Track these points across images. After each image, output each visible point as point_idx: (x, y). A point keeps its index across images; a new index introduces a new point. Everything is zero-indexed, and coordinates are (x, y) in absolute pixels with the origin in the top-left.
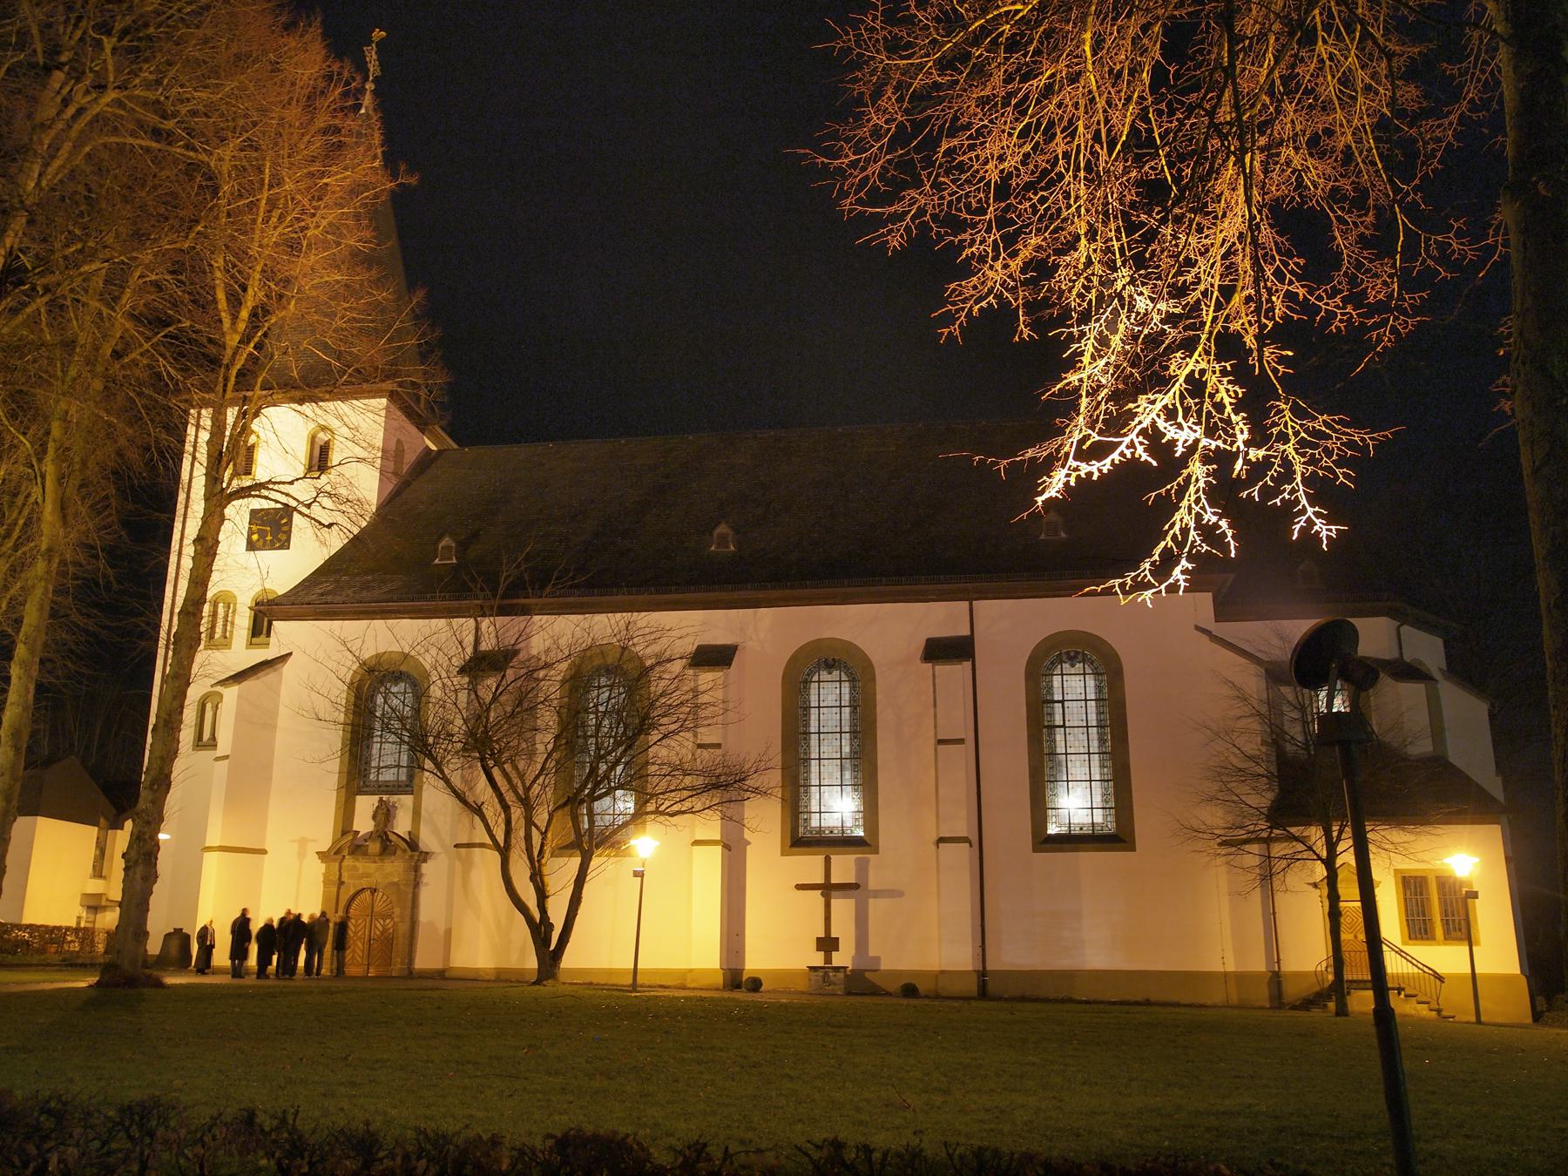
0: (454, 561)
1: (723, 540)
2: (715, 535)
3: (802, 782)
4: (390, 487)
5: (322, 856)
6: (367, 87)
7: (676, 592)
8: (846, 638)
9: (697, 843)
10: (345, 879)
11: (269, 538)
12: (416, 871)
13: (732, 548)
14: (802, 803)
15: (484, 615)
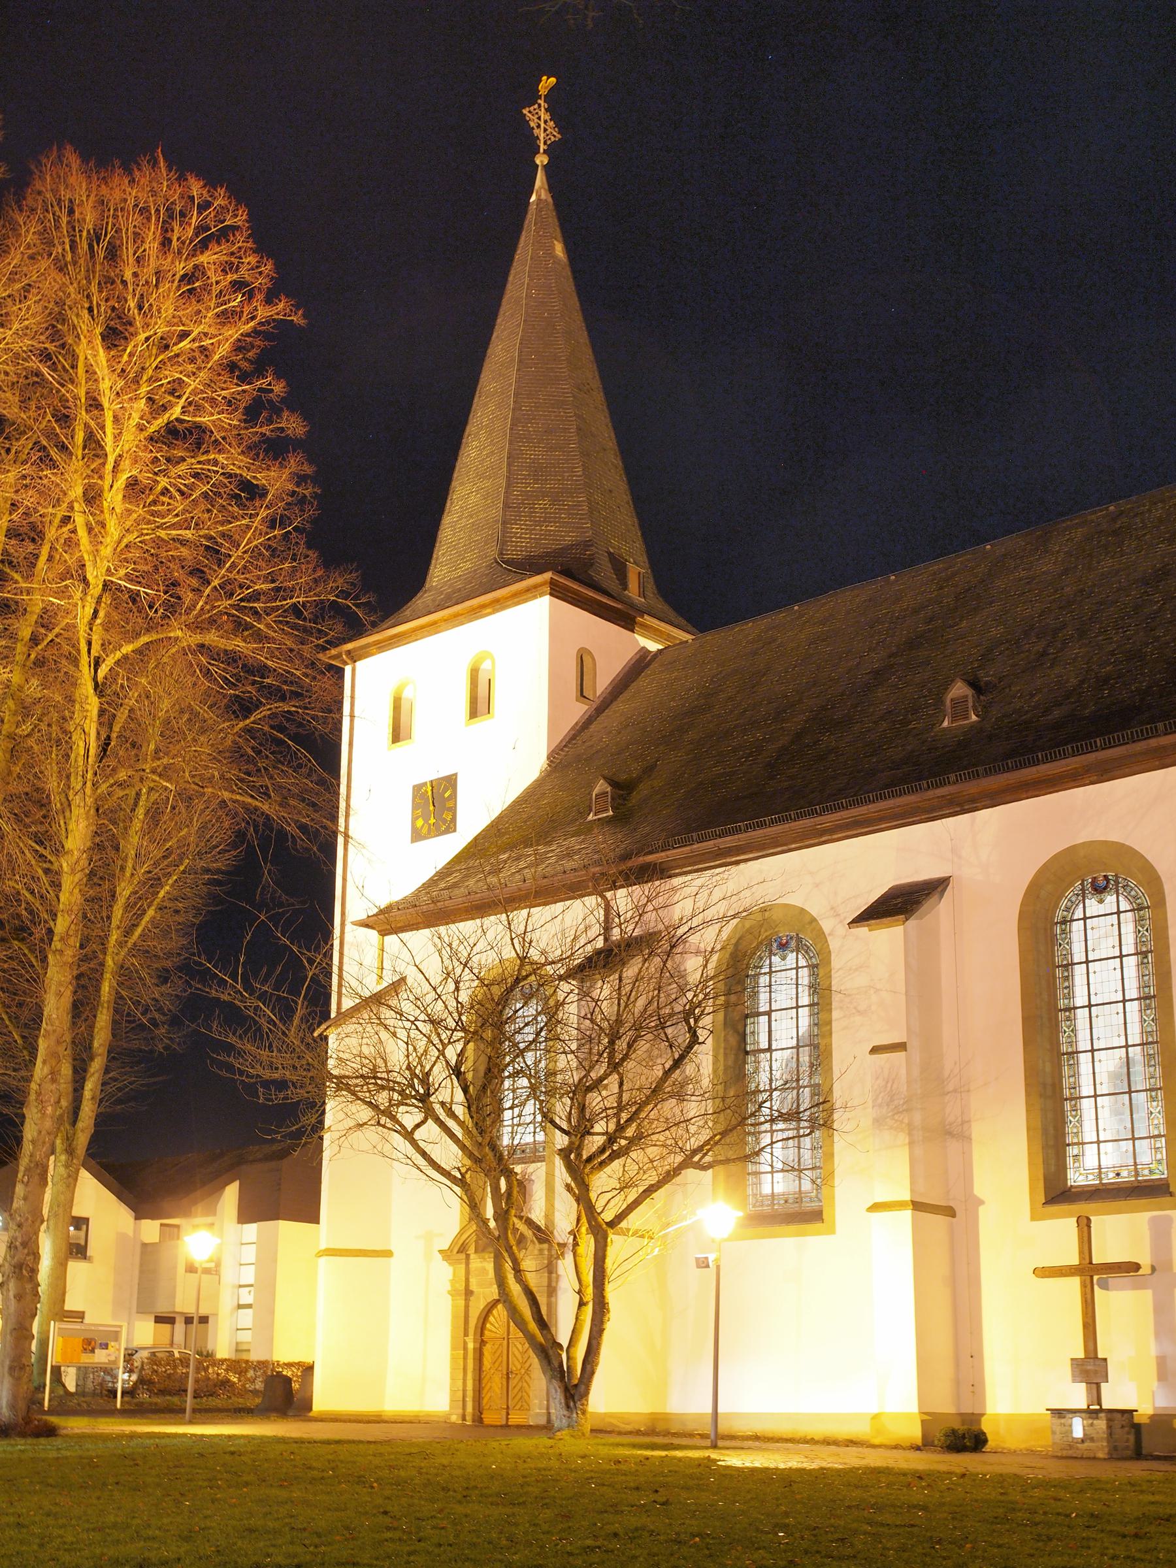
0: (611, 813)
1: (960, 703)
2: (948, 703)
3: (1067, 1093)
4: (578, 711)
5: (446, 1254)
6: (538, 162)
7: (1046, 760)
8: (1114, 837)
9: (876, 1207)
10: (473, 1287)
11: (432, 821)
12: (550, 1273)
13: (974, 718)
14: (1070, 1129)
15: (614, 887)
